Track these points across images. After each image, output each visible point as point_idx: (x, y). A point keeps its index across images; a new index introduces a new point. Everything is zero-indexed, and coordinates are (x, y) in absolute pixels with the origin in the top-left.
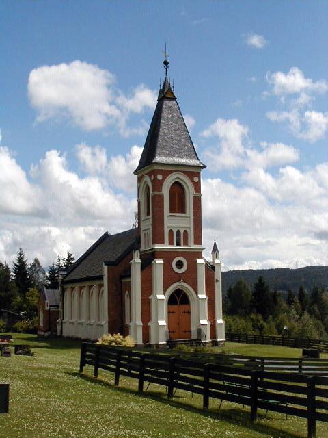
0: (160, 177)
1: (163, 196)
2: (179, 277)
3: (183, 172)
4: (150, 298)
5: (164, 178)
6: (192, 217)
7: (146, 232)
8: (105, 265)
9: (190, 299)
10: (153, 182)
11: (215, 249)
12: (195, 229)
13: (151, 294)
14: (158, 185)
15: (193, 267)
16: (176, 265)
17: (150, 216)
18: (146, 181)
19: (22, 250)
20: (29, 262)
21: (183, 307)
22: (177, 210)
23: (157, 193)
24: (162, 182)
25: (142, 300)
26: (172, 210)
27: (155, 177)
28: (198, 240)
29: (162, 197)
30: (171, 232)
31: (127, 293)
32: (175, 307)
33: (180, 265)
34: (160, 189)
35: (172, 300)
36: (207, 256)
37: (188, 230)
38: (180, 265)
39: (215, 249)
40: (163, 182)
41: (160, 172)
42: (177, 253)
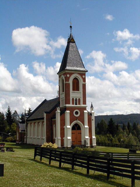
0: (68, 76)
1: (70, 84)
2: (76, 118)
3: (78, 73)
4: (64, 127)
5: (70, 76)
6: (82, 93)
7: (62, 99)
10: (65, 78)
11: (92, 107)
12: (83, 98)
13: (64, 126)
14: (67, 79)
15: (82, 114)
16: (75, 113)
17: (64, 92)
18: (62, 77)
20: (13, 112)
21: (78, 131)
22: (75, 90)
23: (67, 82)
24: (69, 78)
25: (61, 128)
26: (73, 90)
27: (66, 76)
28: (85, 103)
29: (69, 84)
30: (73, 99)
31: (54, 125)
32: (74, 131)
33: (77, 113)
34: (68, 81)
35: (73, 128)
37: (80, 98)
38: (77, 113)
39: (92, 107)
41: (68, 73)
42: (76, 108)
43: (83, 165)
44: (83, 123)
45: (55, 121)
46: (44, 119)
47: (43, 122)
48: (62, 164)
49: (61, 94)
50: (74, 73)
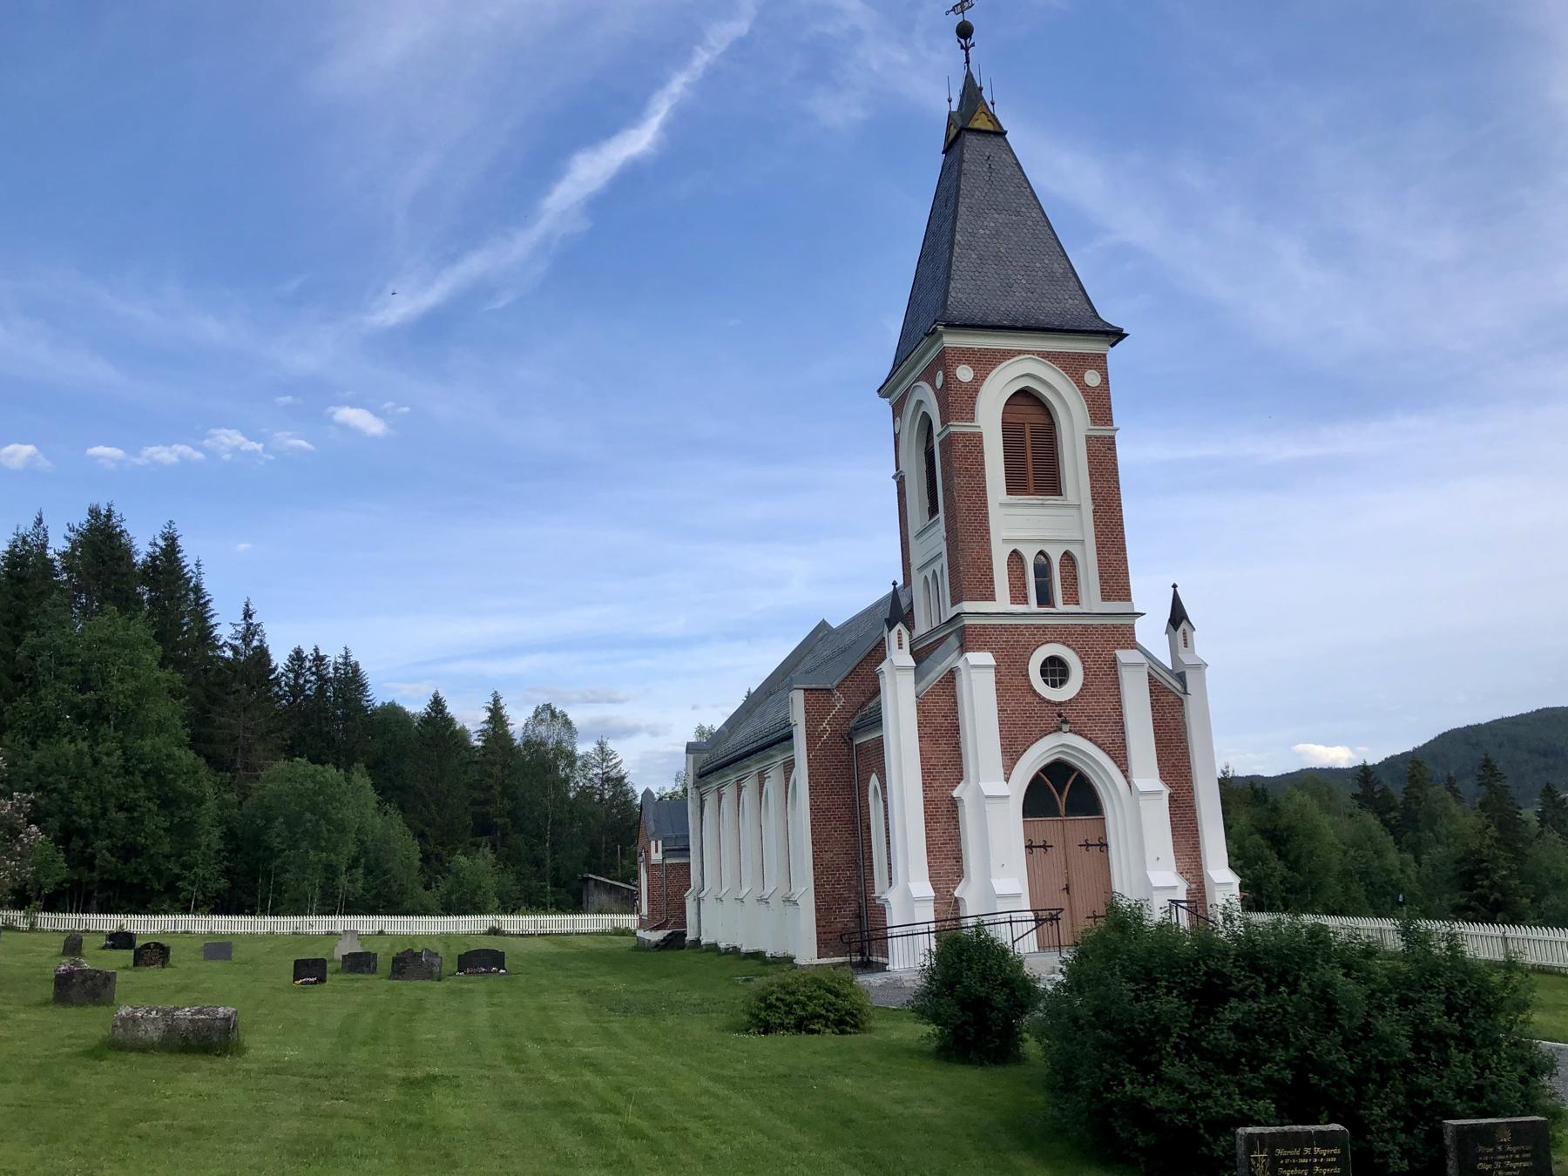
0: (965, 373)
1: (980, 436)
2: (1060, 717)
3: (1047, 355)
4: (955, 794)
5: (979, 379)
6: (1088, 507)
7: (928, 573)
8: (1402, 1133)
9: (1071, 664)
10: (943, 395)
11: (1178, 616)
12: (1100, 547)
13: (960, 779)
14: (957, 401)
15: (1105, 677)
16: (1043, 673)
17: (941, 515)
18: (920, 402)
19: (502, 702)
20: (626, 781)
21: (1079, 826)
22: (1032, 489)
23: (957, 427)
24: (972, 391)
25: (928, 802)
26: (1015, 484)
27: (949, 378)
28: (1116, 583)
29: (976, 441)
30: (1016, 557)
31: (874, 780)
32: (1047, 827)
33: (1055, 670)
34: (970, 414)
35: (1037, 801)
36: (1151, 633)
37: (1075, 550)
38: (1055, 670)
39: (1178, 616)
40: (977, 391)
41: (968, 356)
42: (1043, 634)
43: (1543, 1119)
44: (1120, 756)
45: (879, 746)
46: (789, 737)
47: (789, 766)
48: (934, 934)
49: (920, 534)
50: (1007, 354)
